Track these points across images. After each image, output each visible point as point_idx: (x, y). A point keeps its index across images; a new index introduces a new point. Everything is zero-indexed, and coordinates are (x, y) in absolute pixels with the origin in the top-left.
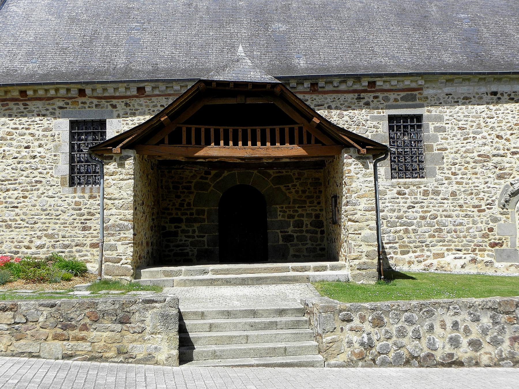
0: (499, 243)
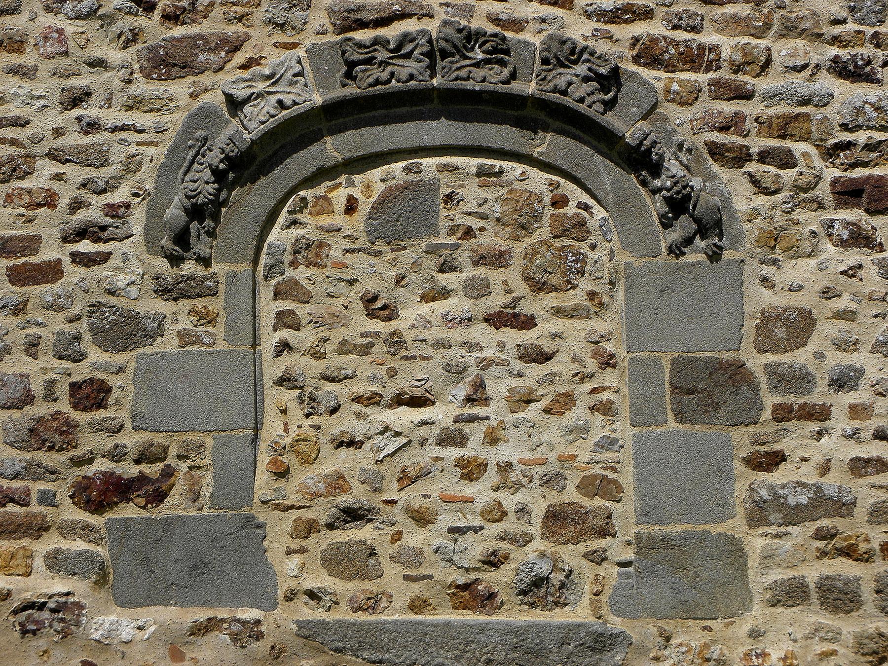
0: (142, 479)
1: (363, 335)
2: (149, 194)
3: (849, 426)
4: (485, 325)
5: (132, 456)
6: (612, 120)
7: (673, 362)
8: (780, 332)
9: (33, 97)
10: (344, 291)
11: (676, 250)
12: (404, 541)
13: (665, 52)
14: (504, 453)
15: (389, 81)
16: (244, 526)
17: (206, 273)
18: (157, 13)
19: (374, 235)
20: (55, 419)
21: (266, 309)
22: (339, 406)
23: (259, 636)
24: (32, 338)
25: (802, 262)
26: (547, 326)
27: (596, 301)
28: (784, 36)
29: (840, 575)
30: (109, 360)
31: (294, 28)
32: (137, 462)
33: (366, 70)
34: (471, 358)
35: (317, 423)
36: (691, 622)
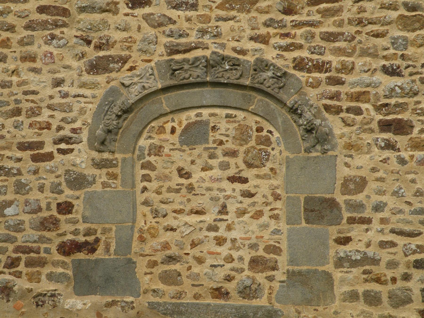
0: (86, 243)
1: (177, 185)
2: (90, 124)
3: (380, 227)
4: (227, 181)
5: (82, 233)
6: (282, 95)
7: (305, 198)
8: (352, 186)
9: (41, 82)
10: (170, 166)
11: (307, 150)
12: (192, 270)
13: (307, 65)
14: (234, 234)
15: (189, 78)
16: (128, 263)
17: (113, 158)
18: (92, 45)
19: (182, 143)
20: (50, 218)
21: (138, 173)
22: (167, 214)
23: (133, 308)
24: (41, 184)
25: (363, 156)
26: (253, 182)
27: (274, 172)
28: (361, 56)
29: (373, 290)
30: (73, 194)
31: (150, 53)
32: (84, 236)
33: (180, 73)
34: (221, 195)
35: (158, 221)
36: (309, 307)
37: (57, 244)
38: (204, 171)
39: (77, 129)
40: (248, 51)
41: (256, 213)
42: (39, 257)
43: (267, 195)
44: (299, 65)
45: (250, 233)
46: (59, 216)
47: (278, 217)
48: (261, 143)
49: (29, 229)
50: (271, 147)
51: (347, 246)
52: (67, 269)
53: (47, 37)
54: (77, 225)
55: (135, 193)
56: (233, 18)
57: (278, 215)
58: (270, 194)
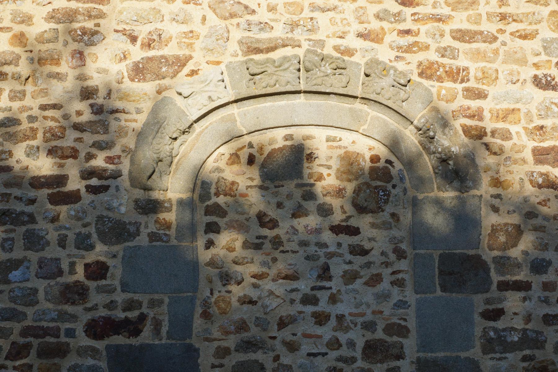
0: (127, 320)
1: (258, 237)
4: (330, 232)
13: (438, 71)
15: (275, 85)
18: (139, 42)
22: (243, 280)
24: (62, 236)
32: (124, 310)
33: (261, 79)
34: (321, 252)
37: (85, 322)
38: (296, 218)
39: (114, 158)
40: (357, 51)
41: (371, 278)
42: (58, 343)
43: (388, 251)
44: (427, 71)
45: (364, 306)
46: (88, 283)
47: (403, 284)
48: (377, 179)
49: (44, 302)
50: (391, 183)
51: (499, 322)
52: (99, 360)
53: (77, 32)
54: (113, 294)
55: (197, 249)
56: (334, 9)
57: (403, 280)
58: (391, 251)
